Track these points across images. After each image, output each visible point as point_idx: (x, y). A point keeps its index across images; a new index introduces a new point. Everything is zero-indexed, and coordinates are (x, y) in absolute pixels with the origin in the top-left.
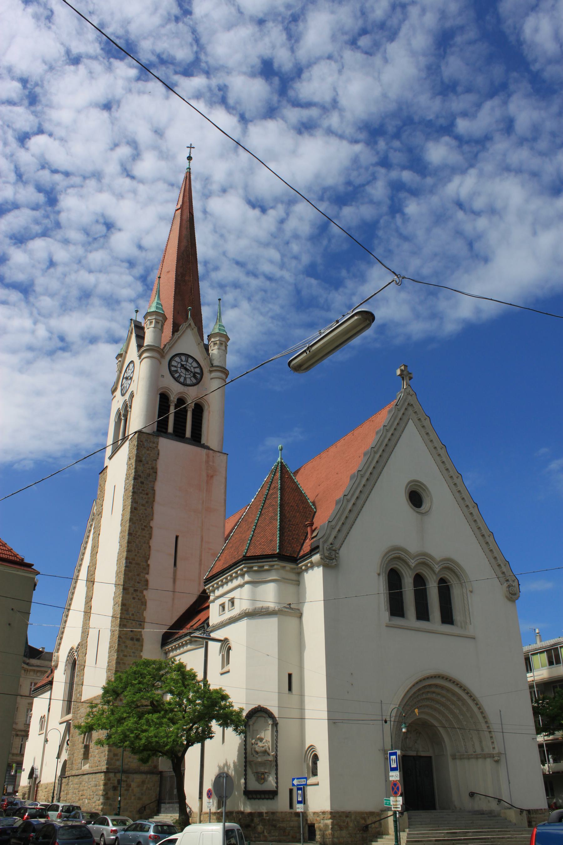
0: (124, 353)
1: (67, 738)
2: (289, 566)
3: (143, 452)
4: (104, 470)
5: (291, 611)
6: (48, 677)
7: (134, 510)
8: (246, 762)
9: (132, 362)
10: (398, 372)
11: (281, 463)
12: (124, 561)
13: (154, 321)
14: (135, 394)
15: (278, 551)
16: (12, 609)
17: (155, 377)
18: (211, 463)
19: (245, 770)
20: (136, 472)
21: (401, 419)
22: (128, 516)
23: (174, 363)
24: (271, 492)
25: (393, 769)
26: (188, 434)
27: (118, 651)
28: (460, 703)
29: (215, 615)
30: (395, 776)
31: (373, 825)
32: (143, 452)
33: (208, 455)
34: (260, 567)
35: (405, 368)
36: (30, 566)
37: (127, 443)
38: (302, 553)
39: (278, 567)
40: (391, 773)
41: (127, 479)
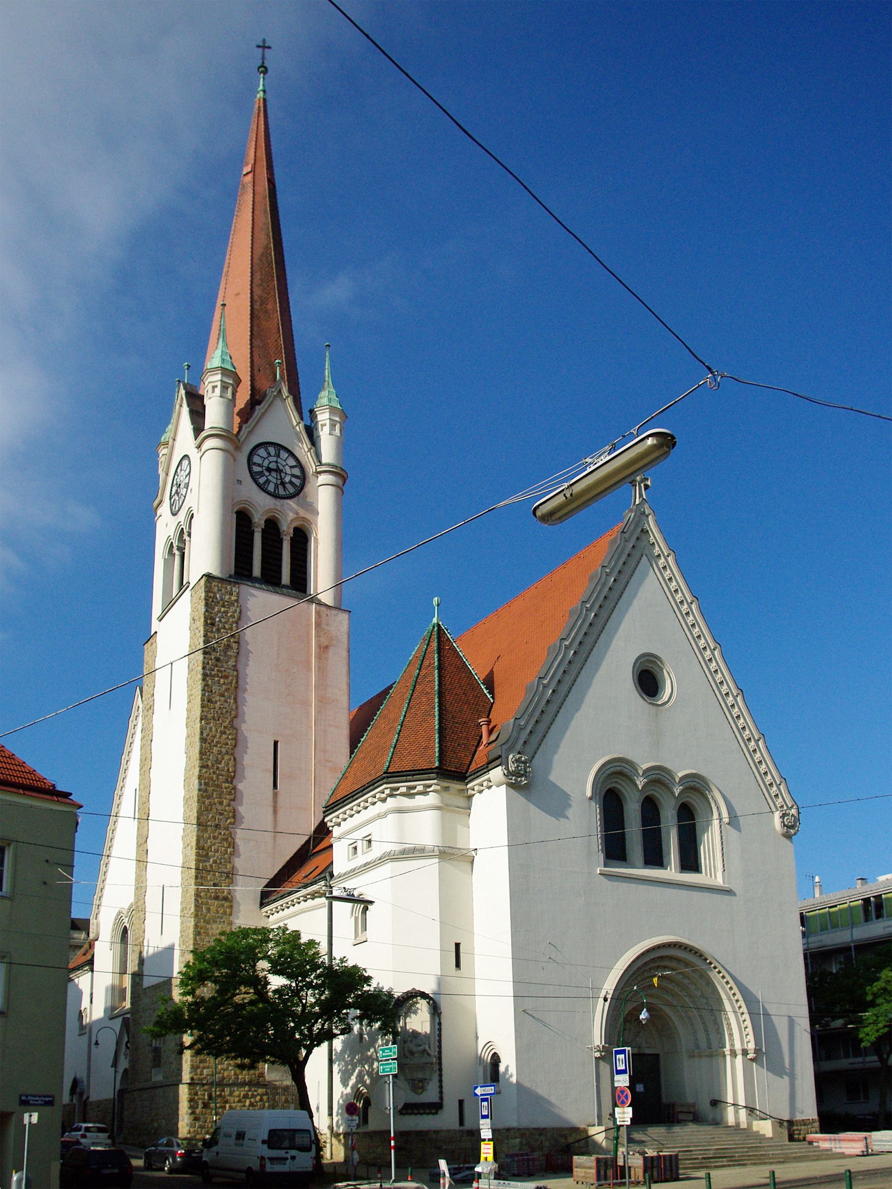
0: (171, 441)
1: (126, 1039)
2: (456, 786)
4: (150, 637)
5: (453, 855)
6: (84, 954)
7: (207, 702)
9: (186, 457)
11: (439, 625)
12: (197, 781)
13: (219, 384)
14: (195, 512)
15: (437, 764)
16: (47, 861)
17: (229, 484)
18: (324, 626)
21: (629, 555)
22: (197, 712)
23: (256, 459)
24: (424, 672)
25: (620, 1072)
26: (286, 578)
28: (686, 981)
29: (341, 859)
30: (622, 1081)
31: (577, 1144)
33: (318, 613)
34: (409, 788)
36: (67, 795)
38: (473, 767)
39: (438, 788)
40: (617, 1077)
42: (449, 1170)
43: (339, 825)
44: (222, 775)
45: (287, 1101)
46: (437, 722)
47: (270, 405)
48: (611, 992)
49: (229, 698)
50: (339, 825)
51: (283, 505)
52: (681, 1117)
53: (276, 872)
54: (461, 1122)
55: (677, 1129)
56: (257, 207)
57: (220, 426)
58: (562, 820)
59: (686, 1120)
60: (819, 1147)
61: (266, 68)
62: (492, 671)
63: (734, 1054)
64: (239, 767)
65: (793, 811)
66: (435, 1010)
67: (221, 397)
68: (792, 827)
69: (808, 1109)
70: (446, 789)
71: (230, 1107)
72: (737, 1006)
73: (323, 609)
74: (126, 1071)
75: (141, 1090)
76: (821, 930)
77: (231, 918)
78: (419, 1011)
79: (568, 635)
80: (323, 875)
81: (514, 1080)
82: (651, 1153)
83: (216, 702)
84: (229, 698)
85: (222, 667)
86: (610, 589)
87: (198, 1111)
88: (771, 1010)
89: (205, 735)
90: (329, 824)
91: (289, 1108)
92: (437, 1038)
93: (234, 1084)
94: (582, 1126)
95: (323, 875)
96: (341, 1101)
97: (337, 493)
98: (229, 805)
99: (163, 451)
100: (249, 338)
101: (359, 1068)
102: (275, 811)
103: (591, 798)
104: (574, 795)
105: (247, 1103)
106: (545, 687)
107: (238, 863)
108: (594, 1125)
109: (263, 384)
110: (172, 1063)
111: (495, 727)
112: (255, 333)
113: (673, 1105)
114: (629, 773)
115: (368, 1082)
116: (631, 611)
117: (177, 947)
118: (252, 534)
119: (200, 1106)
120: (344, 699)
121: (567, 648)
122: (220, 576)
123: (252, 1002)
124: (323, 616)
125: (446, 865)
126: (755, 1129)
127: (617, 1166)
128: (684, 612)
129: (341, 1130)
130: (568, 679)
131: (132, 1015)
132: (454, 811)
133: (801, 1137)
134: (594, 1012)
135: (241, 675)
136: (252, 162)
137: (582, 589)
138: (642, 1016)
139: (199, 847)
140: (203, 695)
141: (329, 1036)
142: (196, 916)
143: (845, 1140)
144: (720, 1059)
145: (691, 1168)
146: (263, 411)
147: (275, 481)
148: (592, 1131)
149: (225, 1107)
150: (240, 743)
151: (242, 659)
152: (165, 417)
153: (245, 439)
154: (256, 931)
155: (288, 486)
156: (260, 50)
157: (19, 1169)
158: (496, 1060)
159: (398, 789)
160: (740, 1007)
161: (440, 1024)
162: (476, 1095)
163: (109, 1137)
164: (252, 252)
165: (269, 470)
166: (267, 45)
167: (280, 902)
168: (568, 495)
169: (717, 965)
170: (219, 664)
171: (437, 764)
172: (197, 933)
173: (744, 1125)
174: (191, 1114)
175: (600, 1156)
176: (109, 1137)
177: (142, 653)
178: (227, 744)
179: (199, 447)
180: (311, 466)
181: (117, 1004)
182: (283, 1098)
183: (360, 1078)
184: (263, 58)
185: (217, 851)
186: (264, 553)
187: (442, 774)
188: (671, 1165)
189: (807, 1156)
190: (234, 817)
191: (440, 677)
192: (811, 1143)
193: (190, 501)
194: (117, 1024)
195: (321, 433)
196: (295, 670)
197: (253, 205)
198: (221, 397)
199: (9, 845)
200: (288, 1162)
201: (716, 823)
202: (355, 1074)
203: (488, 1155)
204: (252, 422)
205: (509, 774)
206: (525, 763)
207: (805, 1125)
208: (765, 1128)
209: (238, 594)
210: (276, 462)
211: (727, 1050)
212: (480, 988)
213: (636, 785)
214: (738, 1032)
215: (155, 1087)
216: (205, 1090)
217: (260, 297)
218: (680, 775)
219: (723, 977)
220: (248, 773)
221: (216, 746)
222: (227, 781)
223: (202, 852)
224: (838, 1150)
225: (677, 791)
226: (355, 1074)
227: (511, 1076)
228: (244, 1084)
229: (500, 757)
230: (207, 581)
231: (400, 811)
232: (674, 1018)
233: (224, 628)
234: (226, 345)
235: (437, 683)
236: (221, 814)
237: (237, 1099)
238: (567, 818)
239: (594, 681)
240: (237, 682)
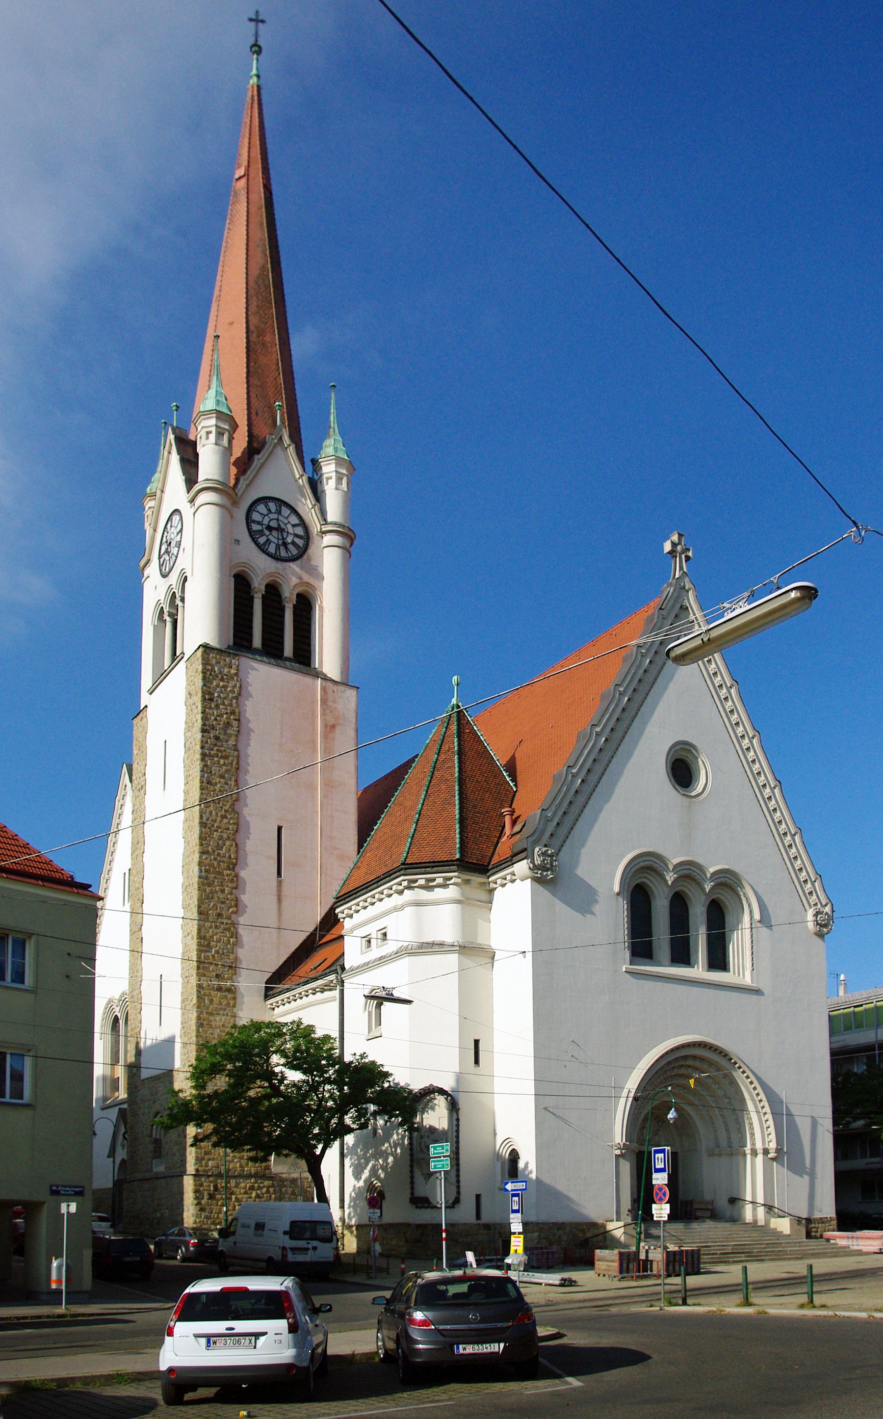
0: (159, 492)
1: (123, 1130)
2: (477, 879)
3: (214, 684)
5: (473, 951)
8: (412, 1160)
9: (176, 511)
10: (667, 547)
12: (197, 868)
13: (213, 429)
14: (188, 574)
15: (458, 856)
16: (69, 954)
17: (227, 543)
18: (330, 703)
19: (412, 1172)
20: (205, 718)
23: (256, 516)
26: (288, 649)
27: (199, 1006)
29: (353, 952)
31: (595, 1239)
32: (214, 684)
33: (324, 689)
35: (679, 539)
36: (86, 887)
37: (182, 666)
39: (459, 880)
41: (188, 729)
42: (476, 1260)
43: (351, 916)
44: (223, 862)
45: (293, 1193)
46: (457, 812)
47: (270, 454)
48: (633, 1091)
49: (230, 780)
50: (351, 916)
51: (285, 569)
52: (698, 1213)
53: (281, 963)
54: (478, 1216)
55: (695, 1226)
56: (251, 220)
57: (216, 478)
58: (588, 916)
59: (703, 1217)
60: (837, 1244)
61: (260, 47)
62: (513, 757)
63: (754, 1153)
64: (241, 853)
65: (827, 909)
66: (454, 1106)
67: (216, 444)
68: (825, 926)
69: (827, 1208)
70: (467, 882)
71: (236, 1198)
72: (760, 1106)
73: (329, 684)
74: (123, 1161)
75: (142, 1180)
76: (845, 1030)
77: (235, 1010)
78: (437, 1107)
79: (600, 721)
80: (333, 968)
81: (533, 1176)
82: (672, 1248)
83: (216, 784)
84: (230, 780)
85: (222, 746)
86: (645, 671)
87: (203, 1202)
88: (794, 1110)
89: (204, 819)
90: (340, 915)
91: (296, 1200)
92: (455, 1134)
93: (240, 1176)
94: (601, 1221)
95: (333, 968)
96: (353, 1194)
97: (343, 555)
98: (231, 893)
99: (150, 504)
100: (245, 375)
101: (372, 1162)
102: (279, 900)
103: (618, 894)
104: (601, 890)
105: (254, 1195)
106: (574, 776)
107: (241, 953)
108: (612, 1221)
109: (262, 430)
110: (175, 1154)
111: (519, 817)
112: (252, 369)
113: (692, 1202)
114: (659, 869)
115: (382, 1176)
116: (666, 695)
117: (178, 1039)
118: (251, 599)
119: (206, 1197)
120: (352, 782)
121: (597, 734)
122: (218, 646)
123: (269, 1097)
124: (330, 692)
125: (469, 962)
126: (772, 1226)
127: (639, 1260)
128: (722, 697)
129: (353, 1222)
130: (598, 768)
131: (129, 1106)
132: (474, 905)
133: (818, 1234)
134: (616, 1111)
135: (242, 755)
136: (245, 163)
137: (614, 672)
138: (670, 1116)
139: (201, 936)
140: (202, 776)
141: (343, 1130)
142: (199, 1007)
143: (862, 1238)
144: (740, 1158)
145: (709, 1263)
146: (262, 461)
147: (276, 541)
148: (610, 1226)
149: (231, 1198)
150: (242, 829)
151: (242, 738)
152: (149, 465)
153: (244, 492)
154: (270, 1025)
155: (290, 547)
156: (253, 24)
157: (59, 1255)
158: (514, 1156)
159: (416, 881)
160: (763, 1107)
161: (458, 1120)
162: (506, 1190)
163: (111, 1226)
164: (247, 274)
165: (270, 528)
166: (261, 18)
167: (287, 995)
168: (705, 640)
169: (742, 1065)
170: (219, 744)
171: (458, 856)
172: (200, 1025)
173: (761, 1222)
174: (196, 1205)
175: (622, 1250)
176: (111, 1226)
177: (131, 728)
178: (228, 829)
179: (192, 501)
180: (315, 526)
181: (109, 1094)
182: (290, 1190)
183: (374, 1172)
184: (257, 35)
185: (219, 941)
186: (265, 621)
187: (463, 867)
188: (693, 1259)
189: (826, 1253)
190: (236, 906)
191: (460, 762)
192: (828, 1240)
193: (183, 562)
194: (114, 1113)
195: (326, 487)
196: (300, 751)
197: (248, 216)
198: (216, 444)
199: (30, 937)
200: (310, 1252)
201: (746, 918)
202: (369, 1168)
203: (517, 1248)
204: (250, 473)
205: (534, 868)
206: (551, 856)
207: (823, 1223)
208: (783, 1225)
209: (238, 666)
210: (278, 520)
211: (748, 1150)
212: (499, 1085)
213: (666, 881)
214: (760, 1132)
215: (157, 1178)
216: (211, 1182)
217: (257, 327)
218: (712, 870)
219: (748, 1077)
220: (251, 860)
221: (217, 831)
222: (228, 868)
223: (204, 943)
224: (856, 1248)
225: (708, 887)
226: (369, 1168)
227: (531, 1172)
228: (249, 1176)
229: (525, 850)
230: (204, 652)
231: (418, 904)
232: (696, 1118)
233: (224, 704)
234: (221, 384)
235: (457, 769)
236: (223, 903)
237: (243, 1191)
238: (594, 914)
239: (626, 771)
240: (238, 762)
